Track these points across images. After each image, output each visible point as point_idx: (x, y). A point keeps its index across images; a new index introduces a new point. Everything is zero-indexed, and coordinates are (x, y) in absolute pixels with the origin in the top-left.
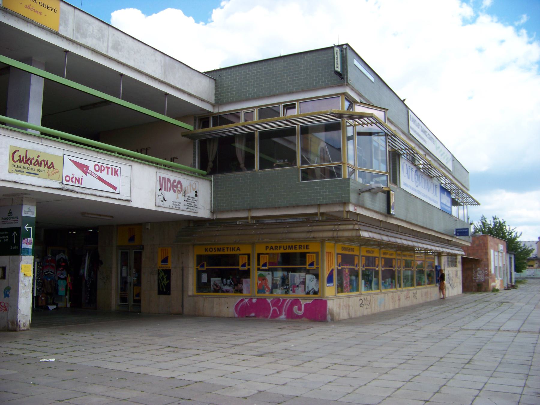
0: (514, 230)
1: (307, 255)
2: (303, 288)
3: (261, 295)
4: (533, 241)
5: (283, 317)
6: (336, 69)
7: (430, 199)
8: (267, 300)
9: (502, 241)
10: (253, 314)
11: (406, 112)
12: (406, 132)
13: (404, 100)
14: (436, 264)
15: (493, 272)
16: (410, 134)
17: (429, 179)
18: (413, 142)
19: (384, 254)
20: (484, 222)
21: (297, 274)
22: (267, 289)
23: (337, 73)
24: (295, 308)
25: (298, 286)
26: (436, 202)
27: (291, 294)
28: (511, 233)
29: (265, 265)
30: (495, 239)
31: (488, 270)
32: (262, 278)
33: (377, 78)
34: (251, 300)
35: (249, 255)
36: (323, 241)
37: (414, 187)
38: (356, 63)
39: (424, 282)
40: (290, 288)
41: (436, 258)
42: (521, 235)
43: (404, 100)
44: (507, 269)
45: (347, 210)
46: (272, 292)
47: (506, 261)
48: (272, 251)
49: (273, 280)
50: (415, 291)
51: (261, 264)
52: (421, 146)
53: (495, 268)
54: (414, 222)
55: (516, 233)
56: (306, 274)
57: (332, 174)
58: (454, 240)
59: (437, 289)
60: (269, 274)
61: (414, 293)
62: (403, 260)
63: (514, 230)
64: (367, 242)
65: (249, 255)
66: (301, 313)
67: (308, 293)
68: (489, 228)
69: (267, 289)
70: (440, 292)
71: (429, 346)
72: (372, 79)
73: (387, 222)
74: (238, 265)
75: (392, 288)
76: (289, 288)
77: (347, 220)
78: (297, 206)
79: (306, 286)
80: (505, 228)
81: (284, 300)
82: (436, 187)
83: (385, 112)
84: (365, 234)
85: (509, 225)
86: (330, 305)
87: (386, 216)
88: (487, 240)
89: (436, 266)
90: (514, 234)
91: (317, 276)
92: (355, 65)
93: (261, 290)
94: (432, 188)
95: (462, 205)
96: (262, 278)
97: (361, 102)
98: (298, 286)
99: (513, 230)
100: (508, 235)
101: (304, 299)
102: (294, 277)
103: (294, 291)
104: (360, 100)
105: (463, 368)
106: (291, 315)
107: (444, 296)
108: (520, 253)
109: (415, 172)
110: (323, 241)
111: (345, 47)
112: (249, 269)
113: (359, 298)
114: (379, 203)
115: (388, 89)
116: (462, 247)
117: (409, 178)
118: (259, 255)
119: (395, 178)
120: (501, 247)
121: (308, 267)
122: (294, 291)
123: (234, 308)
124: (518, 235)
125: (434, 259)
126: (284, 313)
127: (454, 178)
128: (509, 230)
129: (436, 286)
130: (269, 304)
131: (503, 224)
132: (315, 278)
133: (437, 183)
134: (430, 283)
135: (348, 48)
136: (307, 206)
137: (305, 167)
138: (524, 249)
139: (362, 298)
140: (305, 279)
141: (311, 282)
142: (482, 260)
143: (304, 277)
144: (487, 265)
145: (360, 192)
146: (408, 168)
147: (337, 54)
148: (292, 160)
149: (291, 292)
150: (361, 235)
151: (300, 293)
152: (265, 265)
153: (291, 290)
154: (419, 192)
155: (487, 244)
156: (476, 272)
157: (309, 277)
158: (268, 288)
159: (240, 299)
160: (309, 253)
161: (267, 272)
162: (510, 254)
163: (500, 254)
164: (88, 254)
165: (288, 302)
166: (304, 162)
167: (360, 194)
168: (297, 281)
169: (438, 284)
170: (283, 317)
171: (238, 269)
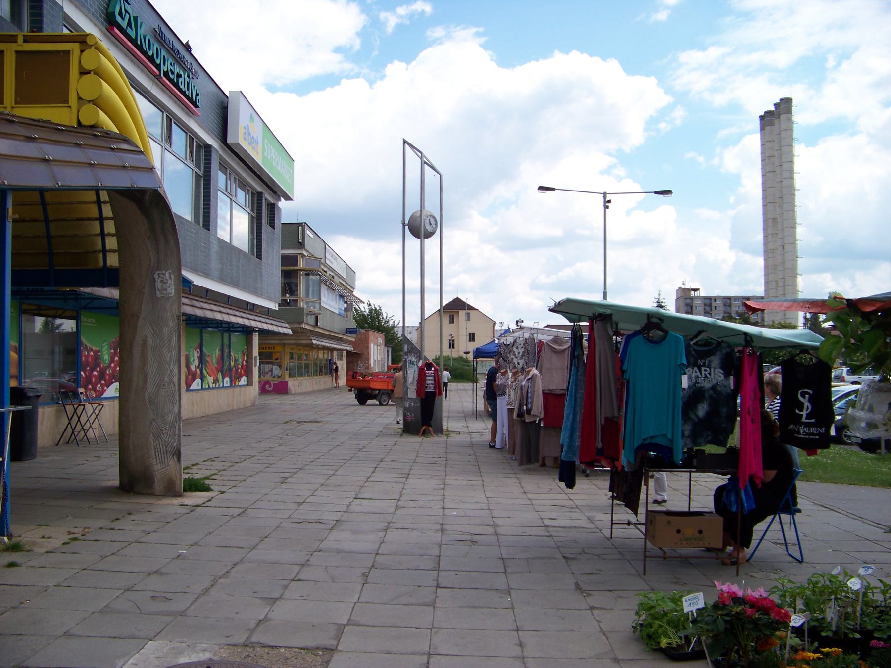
4: (413, 327)
9: (381, 335)
15: (372, 366)
17: (332, 291)
21: (267, 365)
23: (299, 242)
24: (267, 386)
26: (334, 308)
30: (375, 333)
31: (368, 363)
36: (284, 345)
44: (384, 362)
47: (384, 354)
53: (375, 361)
55: (394, 322)
58: (345, 337)
66: (271, 389)
67: (274, 377)
68: (364, 315)
71: (268, 469)
72: (312, 236)
74: (272, 359)
77: (302, 333)
84: (314, 342)
86: (290, 384)
88: (368, 335)
90: (391, 323)
91: (280, 366)
100: (385, 323)
102: (264, 367)
103: (264, 376)
105: (336, 470)
108: (397, 344)
114: (312, 320)
115: (172, 34)
116: (350, 342)
120: (380, 340)
121: (274, 361)
122: (264, 376)
127: (347, 283)
140: (272, 368)
142: (362, 354)
144: (368, 359)
146: (324, 288)
155: (369, 338)
156: (358, 365)
157: (275, 367)
163: (379, 348)
168: (267, 370)
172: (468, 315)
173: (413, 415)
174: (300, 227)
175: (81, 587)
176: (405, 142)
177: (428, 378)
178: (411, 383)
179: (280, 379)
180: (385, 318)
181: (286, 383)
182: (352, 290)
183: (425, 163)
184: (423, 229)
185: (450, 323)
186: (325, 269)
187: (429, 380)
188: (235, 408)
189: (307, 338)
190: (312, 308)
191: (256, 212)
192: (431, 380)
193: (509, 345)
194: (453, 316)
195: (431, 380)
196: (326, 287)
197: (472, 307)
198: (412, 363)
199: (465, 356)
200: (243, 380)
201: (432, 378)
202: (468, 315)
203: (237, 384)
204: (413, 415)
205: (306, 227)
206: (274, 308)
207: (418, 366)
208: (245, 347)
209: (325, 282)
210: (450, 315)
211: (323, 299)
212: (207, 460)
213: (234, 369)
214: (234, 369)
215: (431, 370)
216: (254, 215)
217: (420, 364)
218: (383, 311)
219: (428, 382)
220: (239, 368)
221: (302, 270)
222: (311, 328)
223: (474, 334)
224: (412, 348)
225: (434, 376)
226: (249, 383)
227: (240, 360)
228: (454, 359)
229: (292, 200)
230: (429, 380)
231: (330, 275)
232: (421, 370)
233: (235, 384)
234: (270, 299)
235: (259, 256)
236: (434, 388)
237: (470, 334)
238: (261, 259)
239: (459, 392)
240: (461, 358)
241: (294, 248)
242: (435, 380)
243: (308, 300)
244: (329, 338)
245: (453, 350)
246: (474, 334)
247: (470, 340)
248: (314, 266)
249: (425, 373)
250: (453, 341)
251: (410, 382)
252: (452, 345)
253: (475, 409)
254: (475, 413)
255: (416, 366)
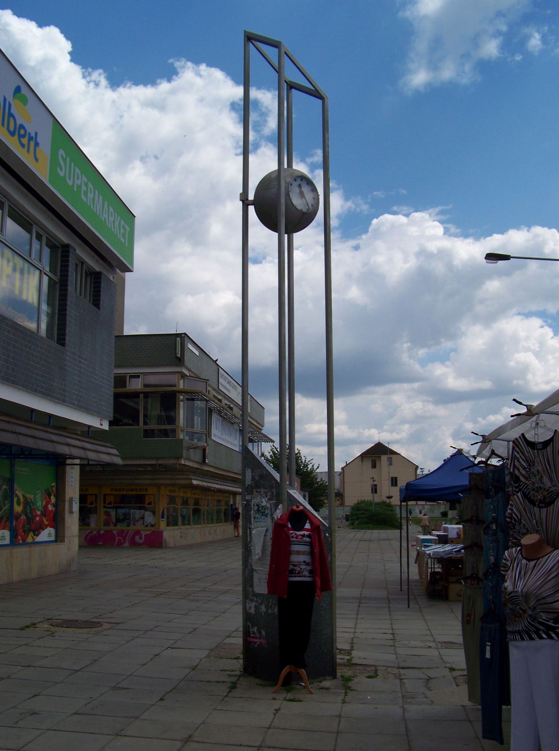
0: (310, 462)
1: (146, 496)
2: (142, 522)
3: (107, 528)
5: (127, 544)
6: (177, 355)
7: (231, 444)
8: (113, 531)
10: (100, 543)
11: (217, 370)
12: (217, 389)
13: (217, 360)
14: (232, 503)
16: (220, 389)
18: (221, 395)
19: (194, 494)
20: (275, 452)
22: (111, 523)
24: (137, 538)
25: (138, 520)
27: (132, 527)
28: (307, 466)
29: (110, 503)
32: (108, 514)
33: (200, 350)
34: (99, 531)
35: (96, 495)
36: (159, 486)
37: (221, 436)
38: (190, 346)
39: (221, 520)
40: (131, 522)
41: (231, 496)
42: (318, 467)
43: (217, 360)
45: (180, 463)
46: (115, 525)
48: (116, 493)
49: (116, 515)
50: (215, 528)
51: (107, 503)
52: (226, 397)
54: (219, 467)
55: (313, 466)
56: (145, 511)
57: (165, 433)
59: (232, 526)
60: (113, 511)
61: (215, 530)
62: (193, 498)
63: (310, 462)
64: (197, 487)
65: (96, 495)
67: (146, 526)
69: (111, 523)
70: (235, 528)
72: (197, 353)
73: (202, 469)
74: (145, 504)
75: (198, 524)
76: (130, 522)
78: (140, 458)
79: (145, 520)
80: (300, 459)
81: (128, 532)
82: (236, 431)
83: (207, 382)
84: (195, 482)
85: (304, 456)
86: (166, 535)
87: (201, 464)
89: (232, 505)
90: (310, 467)
91: (154, 513)
92: (189, 348)
93: (106, 523)
94: (233, 434)
95: (256, 442)
96: (108, 514)
97: (190, 376)
98: (138, 520)
99: (309, 461)
100: (304, 467)
101: (144, 530)
103: (134, 525)
104: (189, 374)
106: (134, 544)
107: (238, 535)
109: (222, 423)
110: (159, 486)
111: (183, 335)
112: (96, 507)
113: (180, 531)
114: (196, 456)
117: (217, 429)
118: (105, 495)
119: (209, 433)
121: (147, 506)
122: (134, 525)
123: (84, 538)
124: (315, 467)
125: (229, 497)
126: (127, 542)
128: (305, 462)
129: (231, 524)
130: (115, 535)
131: (298, 454)
132: (152, 514)
133: (237, 427)
134: (226, 521)
135: (186, 336)
136: (147, 459)
137: (146, 427)
138: (321, 484)
139: (182, 531)
140: (144, 515)
141: (149, 518)
143: (143, 514)
145: (189, 448)
147: (178, 343)
148: (136, 420)
149: (132, 525)
150: (193, 483)
151: (139, 526)
152: (110, 503)
153: (132, 524)
154: (224, 440)
157: (147, 513)
158: (113, 522)
159: (89, 531)
160: (147, 495)
161: (111, 510)
162: (305, 491)
164: (396, 515)
165: (131, 533)
166: (145, 423)
167: (188, 450)
168: (138, 516)
169: (232, 523)
170: (127, 544)
171: (144, 506)
172: (390, 460)
173: (263, 633)
174: (178, 339)
175: (98, 673)
176: (250, 38)
177: (295, 548)
178: (259, 559)
179: (153, 529)
180: (304, 461)
181: (160, 534)
182: (261, 428)
183: (291, 86)
184: (283, 200)
185: (372, 468)
186: (220, 397)
187: (298, 553)
188: (15, 578)
189: (185, 477)
190: (196, 441)
191: (59, 274)
192: (303, 553)
193: (546, 444)
194: (375, 461)
195: (303, 553)
196: (221, 419)
197: (395, 452)
198: (261, 510)
199: (388, 501)
200: (47, 534)
201: (306, 548)
202: (390, 460)
203: (30, 540)
204: (263, 633)
205: (186, 339)
206: (98, 426)
207: (273, 518)
208: (54, 484)
209: (219, 413)
210: (372, 462)
211: (214, 431)
212: (113, 612)
213: (23, 517)
214: (23, 517)
215: (302, 529)
216: (56, 279)
217: (278, 513)
218: (302, 455)
219: (295, 558)
220: (37, 515)
221: (181, 392)
222: (195, 466)
223: (396, 478)
224: (261, 477)
225: (311, 545)
226: (59, 538)
227: (40, 504)
228: (377, 504)
229: (132, 272)
230: (298, 553)
231: (226, 404)
232: (279, 528)
233: (24, 540)
234: (102, 417)
235: (61, 341)
236: (311, 572)
237: (392, 478)
238: (63, 345)
239: (381, 542)
240: (384, 503)
241: (171, 365)
242: (312, 553)
243: (190, 430)
244: (233, 481)
245: (375, 495)
246: (396, 478)
247: (392, 485)
248: (199, 387)
249: (288, 537)
250: (376, 485)
251: (257, 557)
252: (374, 489)
253: (405, 576)
254: (405, 587)
255: (269, 519)
